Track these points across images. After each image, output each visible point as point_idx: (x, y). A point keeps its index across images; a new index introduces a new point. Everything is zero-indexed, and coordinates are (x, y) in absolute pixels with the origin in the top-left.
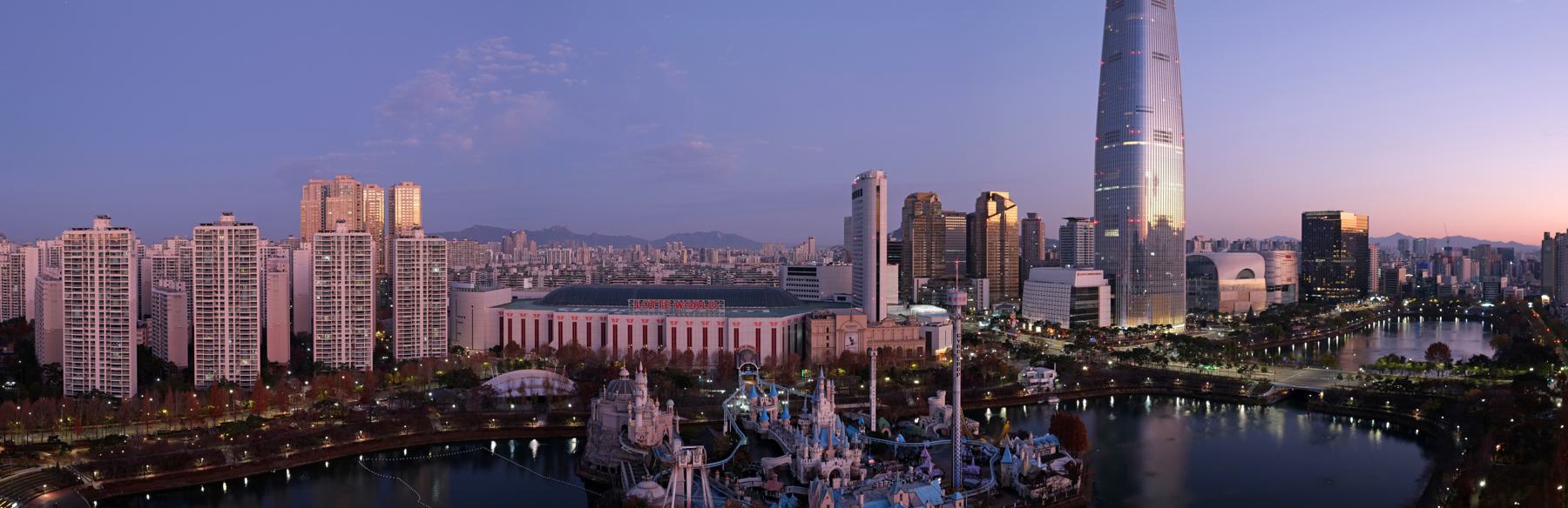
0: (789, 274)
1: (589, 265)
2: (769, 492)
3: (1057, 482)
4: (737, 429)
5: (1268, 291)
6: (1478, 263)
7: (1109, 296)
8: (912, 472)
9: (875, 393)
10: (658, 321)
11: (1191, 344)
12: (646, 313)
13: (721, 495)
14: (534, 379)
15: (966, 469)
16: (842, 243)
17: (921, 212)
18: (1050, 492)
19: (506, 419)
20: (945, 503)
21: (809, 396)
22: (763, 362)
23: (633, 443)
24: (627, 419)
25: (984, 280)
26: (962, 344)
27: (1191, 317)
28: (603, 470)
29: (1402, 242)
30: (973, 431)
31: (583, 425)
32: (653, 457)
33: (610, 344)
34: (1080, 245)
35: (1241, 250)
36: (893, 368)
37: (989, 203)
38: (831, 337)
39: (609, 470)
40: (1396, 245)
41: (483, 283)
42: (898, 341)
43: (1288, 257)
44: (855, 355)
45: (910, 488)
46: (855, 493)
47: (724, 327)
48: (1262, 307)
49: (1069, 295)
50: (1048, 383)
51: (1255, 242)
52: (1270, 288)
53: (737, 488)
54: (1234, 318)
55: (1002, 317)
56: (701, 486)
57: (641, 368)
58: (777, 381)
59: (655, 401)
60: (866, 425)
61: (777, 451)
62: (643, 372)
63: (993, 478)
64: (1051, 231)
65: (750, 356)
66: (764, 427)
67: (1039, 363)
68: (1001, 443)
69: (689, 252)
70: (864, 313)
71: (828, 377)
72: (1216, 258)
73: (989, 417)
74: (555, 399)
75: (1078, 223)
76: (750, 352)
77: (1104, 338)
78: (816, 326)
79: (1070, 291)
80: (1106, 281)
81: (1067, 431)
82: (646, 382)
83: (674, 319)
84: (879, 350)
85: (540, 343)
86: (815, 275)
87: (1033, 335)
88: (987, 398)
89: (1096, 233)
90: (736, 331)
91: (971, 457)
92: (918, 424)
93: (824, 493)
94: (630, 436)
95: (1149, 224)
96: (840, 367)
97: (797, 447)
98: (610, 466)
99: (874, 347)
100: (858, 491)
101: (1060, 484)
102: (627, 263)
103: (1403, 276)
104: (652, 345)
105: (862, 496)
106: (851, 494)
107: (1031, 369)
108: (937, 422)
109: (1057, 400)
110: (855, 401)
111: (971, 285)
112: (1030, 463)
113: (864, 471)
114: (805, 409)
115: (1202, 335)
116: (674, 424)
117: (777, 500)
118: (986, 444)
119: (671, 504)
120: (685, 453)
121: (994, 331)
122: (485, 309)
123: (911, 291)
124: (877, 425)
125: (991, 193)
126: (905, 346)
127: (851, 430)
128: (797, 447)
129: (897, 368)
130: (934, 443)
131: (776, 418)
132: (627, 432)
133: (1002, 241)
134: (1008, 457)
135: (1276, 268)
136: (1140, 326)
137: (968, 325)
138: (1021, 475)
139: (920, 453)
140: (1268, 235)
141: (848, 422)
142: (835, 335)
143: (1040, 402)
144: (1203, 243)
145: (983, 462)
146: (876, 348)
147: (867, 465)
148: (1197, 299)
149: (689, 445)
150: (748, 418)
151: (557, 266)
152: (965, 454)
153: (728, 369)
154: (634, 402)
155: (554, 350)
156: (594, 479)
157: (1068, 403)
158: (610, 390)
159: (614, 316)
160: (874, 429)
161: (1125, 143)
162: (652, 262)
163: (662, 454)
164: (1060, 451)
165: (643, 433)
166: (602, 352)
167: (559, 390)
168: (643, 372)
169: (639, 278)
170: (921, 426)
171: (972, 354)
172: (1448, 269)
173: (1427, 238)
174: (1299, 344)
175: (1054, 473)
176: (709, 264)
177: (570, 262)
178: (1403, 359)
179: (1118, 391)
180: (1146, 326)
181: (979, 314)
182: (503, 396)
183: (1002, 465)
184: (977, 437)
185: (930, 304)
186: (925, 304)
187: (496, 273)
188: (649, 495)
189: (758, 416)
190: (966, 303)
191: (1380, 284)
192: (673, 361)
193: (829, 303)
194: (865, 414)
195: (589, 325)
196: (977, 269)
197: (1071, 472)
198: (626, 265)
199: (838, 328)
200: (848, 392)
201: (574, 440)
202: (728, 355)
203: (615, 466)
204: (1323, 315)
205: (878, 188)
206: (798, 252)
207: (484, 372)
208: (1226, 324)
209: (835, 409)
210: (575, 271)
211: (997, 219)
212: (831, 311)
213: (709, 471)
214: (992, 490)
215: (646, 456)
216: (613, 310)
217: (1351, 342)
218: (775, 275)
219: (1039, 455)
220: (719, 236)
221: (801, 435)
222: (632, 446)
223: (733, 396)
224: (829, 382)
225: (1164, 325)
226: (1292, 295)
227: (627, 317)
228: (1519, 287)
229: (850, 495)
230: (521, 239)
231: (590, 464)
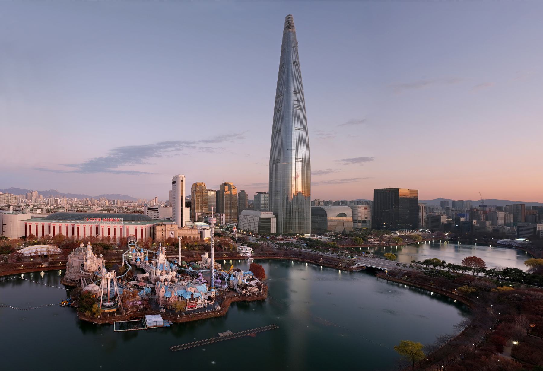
0: (148, 210)
1: (67, 205)
4: (128, 264)
5: (354, 222)
8: (195, 281)
10: (96, 226)
12: (91, 223)
13: (121, 288)
14: (42, 249)
17: (199, 190)
18: (250, 292)
19: (29, 266)
22: (138, 240)
23: (86, 270)
24: (83, 261)
25: (223, 214)
26: (215, 236)
28: (73, 281)
29: (444, 203)
30: (219, 267)
32: (94, 275)
33: (76, 234)
39: (76, 281)
41: (16, 211)
46: (173, 287)
47: (123, 228)
49: (258, 221)
51: (347, 202)
52: (355, 221)
53: (128, 285)
54: (335, 233)
56: (114, 285)
57: (89, 243)
58: (143, 247)
59: (95, 255)
60: (177, 263)
61: (143, 272)
63: (227, 285)
65: (133, 238)
66: (138, 263)
67: (245, 245)
68: (230, 273)
69: (109, 201)
70: (176, 224)
71: (163, 246)
73: (225, 263)
74: (52, 256)
75: (262, 194)
76: (133, 237)
77: (273, 237)
78: (158, 228)
80: (274, 216)
81: (257, 271)
82: (91, 248)
83: (103, 225)
84: (182, 237)
85: (45, 235)
86: (158, 210)
88: (224, 256)
90: (127, 230)
92: (197, 264)
93: (161, 287)
94: (84, 268)
96: (167, 242)
97: (151, 271)
98: (76, 279)
99: (181, 236)
100: (174, 286)
102: (83, 204)
104: (94, 234)
105: (176, 288)
106: (172, 287)
107: (242, 247)
108: (205, 263)
109: (253, 259)
110: (173, 255)
113: (177, 279)
114: (154, 257)
116: (103, 263)
117: (143, 289)
118: (224, 273)
119: (101, 292)
120: (107, 273)
121: (227, 233)
122: (18, 221)
123: (195, 217)
124: (182, 263)
126: (192, 236)
127: (172, 265)
129: (189, 244)
130: (203, 271)
132: (83, 266)
133: (231, 201)
134: (232, 278)
137: (217, 230)
138: (238, 285)
140: (355, 198)
141: (171, 262)
143: (245, 259)
145: (223, 279)
146: (181, 236)
147: (178, 277)
150: (132, 260)
151: (52, 205)
152: (216, 275)
153: (124, 243)
154: (86, 255)
155: (51, 237)
156: (69, 285)
158: (76, 251)
159: (78, 224)
160: (180, 265)
162: (94, 205)
163: (98, 274)
164: (254, 278)
167: (53, 252)
168: (90, 244)
169: (88, 210)
170: (198, 264)
171: (218, 240)
173: (464, 200)
175: (251, 286)
176: (116, 206)
177: (58, 204)
181: (221, 226)
182: (27, 256)
184: (220, 270)
185: (202, 222)
188: (93, 289)
189: (136, 260)
190: (216, 222)
192: (102, 240)
193: (163, 220)
194: (177, 260)
195: (67, 228)
197: (259, 286)
198: (83, 205)
199: (166, 229)
200: (170, 252)
201: (61, 271)
202: (124, 238)
203: (78, 279)
204: (388, 236)
205: (182, 181)
206: (151, 202)
207: (18, 247)
209: (166, 257)
210: (60, 207)
212: (164, 223)
213: (117, 279)
216: (77, 222)
218: (142, 210)
220: (120, 195)
221: (152, 266)
222: (86, 272)
224: (163, 248)
227: (83, 224)
229: (171, 287)
230: (35, 194)
231: (67, 279)
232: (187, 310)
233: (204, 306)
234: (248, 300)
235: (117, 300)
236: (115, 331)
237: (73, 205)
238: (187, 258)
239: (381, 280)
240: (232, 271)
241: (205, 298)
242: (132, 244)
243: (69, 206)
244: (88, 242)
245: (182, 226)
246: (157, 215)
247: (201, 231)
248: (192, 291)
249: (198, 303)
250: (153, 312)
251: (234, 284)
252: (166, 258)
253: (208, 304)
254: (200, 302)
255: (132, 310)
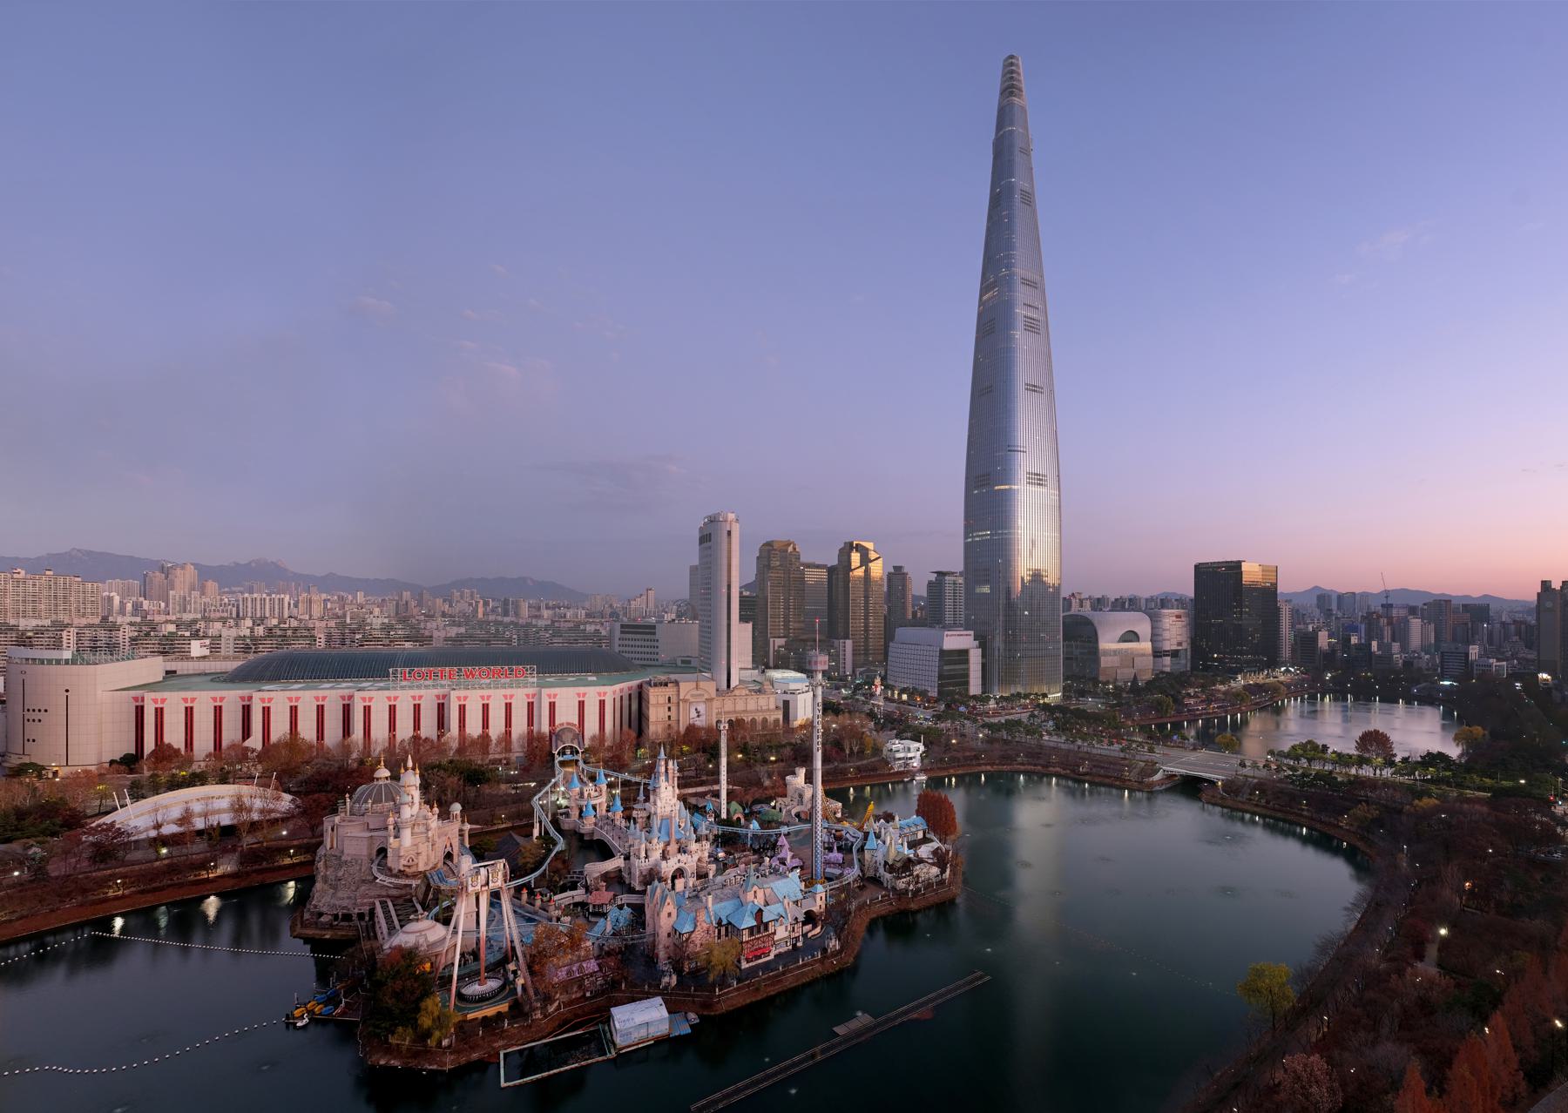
0: (622, 632)
1: (321, 619)
2: (594, 906)
3: (925, 870)
4: (552, 831)
5: (1154, 657)
6: (1433, 625)
7: (980, 659)
9: (725, 773)
11: (1068, 715)
12: (419, 687)
13: (530, 920)
15: (828, 857)
16: (686, 595)
17: (778, 563)
18: (917, 883)
20: (804, 898)
21: (647, 781)
23: (395, 871)
24: (386, 838)
25: (847, 641)
26: (823, 713)
27: (1069, 685)
28: (343, 920)
29: (1323, 598)
30: (835, 813)
31: (311, 859)
32: (428, 887)
34: (949, 602)
35: (1123, 609)
36: (746, 744)
37: (852, 554)
38: (673, 709)
40: (1315, 601)
42: (751, 712)
43: (1178, 617)
44: (703, 728)
45: (766, 883)
47: (535, 700)
48: (1149, 676)
50: (914, 757)
51: (1140, 599)
52: (1158, 653)
53: (552, 908)
54: (1116, 687)
55: (865, 684)
56: (501, 913)
57: (410, 764)
58: (606, 766)
59: (432, 807)
60: (715, 812)
61: (605, 852)
62: (414, 769)
63: (856, 866)
64: (918, 587)
65: (570, 736)
66: (588, 825)
68: (865, 827)
69: (486, 604)
70: (713, 680)
71: (670, 756)
72: (1096, 617)
74: (254, 826)
75: (947, 578)
76: (570, 730)
78: (656, 697)
79: (938, 654)
81: (935, 814)
83: (462, 693)
84: (730, 722)
86: (654, 634)
87: (899, 703)
89: (966, 589)
90: (552, 706)
91: (832, 843)
92: (774, 807)
93: (664, 898)
94: (391, 862)
95: (1023, 579)
96: (684, 744)
97: (630, 846)
98: (356, 911)
99: (725, 719)
101: (928, 873)
103: (1324, 640)
104: (428, 729)
105: (710, 898)
106: (697, 896)
107: (897, 742)
108: (795, 803)
110: (702, 784)
111: (832, 647)
112: (896, 849)
113: (713, 867)
114: (641, 797)
115: (1081, 707)
116: (461, 836)
118: (849, 829)
120: (478, 873)
121: (858, 699)
124: (728, 811)
125: (855, 543)
127: (697, 818)
128: (630, 846)
130: (792, 828)
131: (604, 812)
132: (386, 857)
133: (867, 597)
134: (872, 843)
135: (1164, 630)
136: (1012, 695)
138: (886, 863)
139: (777, 841)
141: (694, 809)
142: (679, 706)
143: (906, 780)
144: (1081, 601)
145: (846, 849)
147: (716, 860)
148: (1074, 665)
149: (483, 860)
150: (567, 815)
152: (826, 840)
155: (253, 751)
156: (327, 937)
157: (936, 783)
158: (358, 801)
159: (366, 694)
160: (724, 816)
161: (996, 488)
162: (430, 617)
163: (442, 880)
164: (928, 836)
165: (412, 854)
166: (343, 746)
167: (262, 811)
168: (414, 769)
169: (408, 639)
170: (778, 808)
172: (1387, 632)
174: (1192, 722)
175: (921, 861)
177: (286, 615)
178: (1325, 748)
179: (989, 768)
180: (1019, 694)
182: (143, 836)
183: (866, 851)
184: (839, 821)
186: (782, 668)
187: (127, 633)
191: (1293, 651)
192: (460, 750)
194: (714, 799)
196: (840, 629)
197: (940, 859)
198: (386, 621)
199: (681, 697)
201: (292, 884)
202: (541, 737)
203: (366, 909)
204: (1222, 688)
205: (729, 533)
208: (1107, 693)
210: (295, 630)
211: (860, 572)
212: (673, 677)
213: (512, 891)
214: (855, 881)
215: (417, 886)
217: (1256, 723)
218: (604, 633)
219: (906, 839)
222: (396, 876)
223: (547, 788)
224: (670, 763)
225: (1039, 693)
226: (1183, 662)
227: (387, 693)
228: (1498, 660)
229: (695, 897)
230: (184, 579)
231: (321, 914)
232: (745, 965)
233: (794, 946)
234: (913, 906)
235: (512, 967)
236: (503, 1084)
237: (348, 621)
238: (745, 791)
239: (1210, 807)
240: (872, 820)
241: (796, 918)
242: (568, 757)
243: (332, 624)
244: (405, 761)
245: (729, 686)
246: (652, 650)
247: (787, 697)
248: (759, 902)
249: (776, 938)
250: (638, 993)
251: (876, 862)
252: (678, 799)
253: (805, 935)
254: (781, 933)
255: (565, 998)
